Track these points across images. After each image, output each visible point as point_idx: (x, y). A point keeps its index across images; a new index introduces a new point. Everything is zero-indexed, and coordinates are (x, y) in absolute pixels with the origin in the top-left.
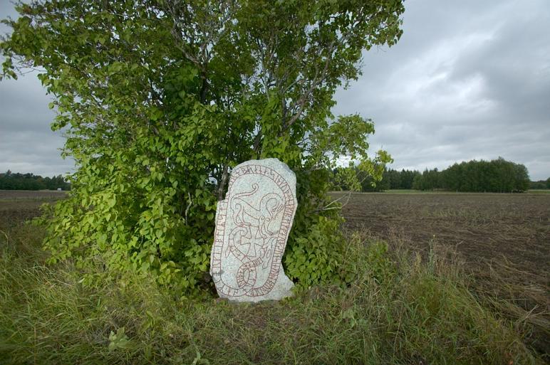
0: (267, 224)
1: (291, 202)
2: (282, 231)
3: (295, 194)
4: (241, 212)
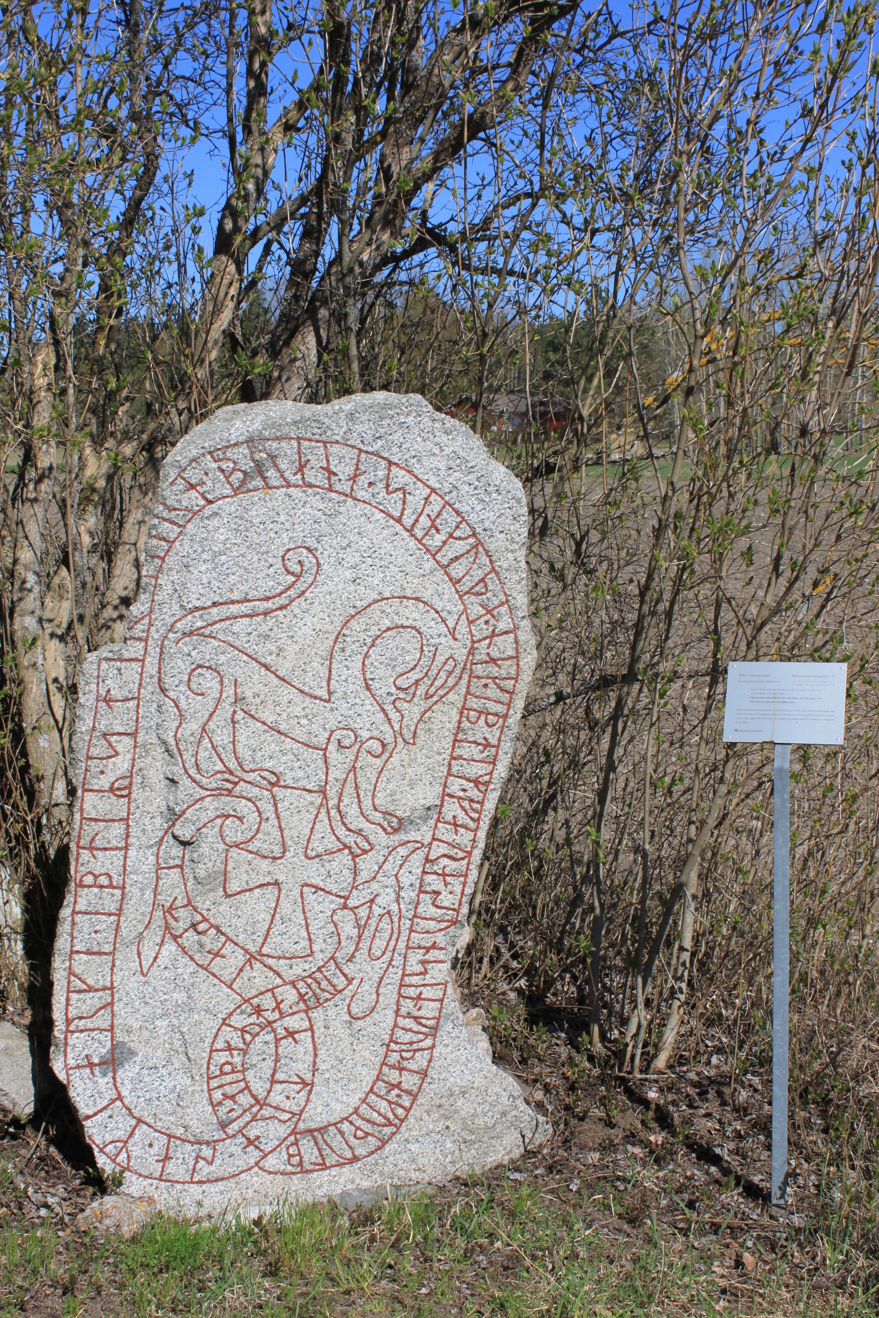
0: (370, 765)
1: (505, 645)
2: (452, 809)
3: (521, 600)
4: (226, 710)
